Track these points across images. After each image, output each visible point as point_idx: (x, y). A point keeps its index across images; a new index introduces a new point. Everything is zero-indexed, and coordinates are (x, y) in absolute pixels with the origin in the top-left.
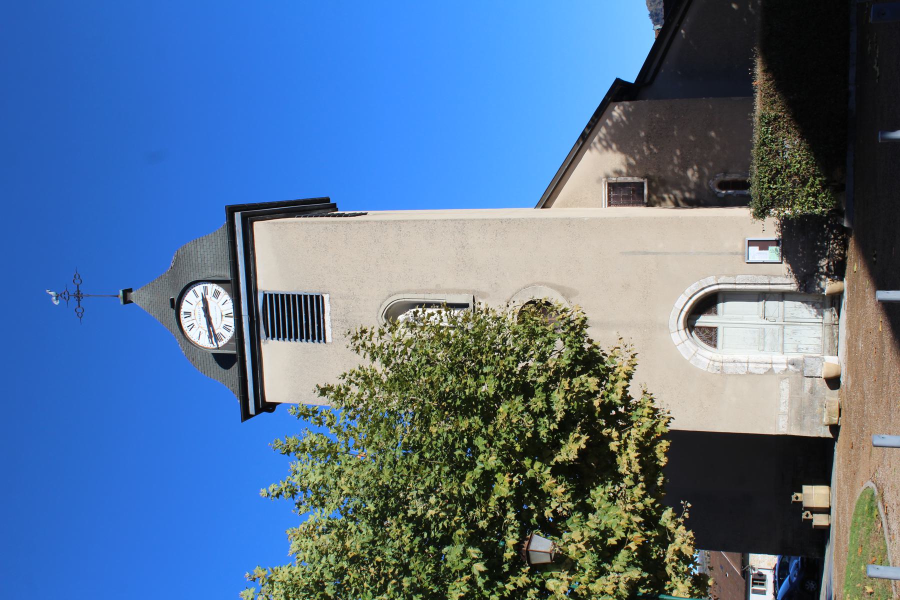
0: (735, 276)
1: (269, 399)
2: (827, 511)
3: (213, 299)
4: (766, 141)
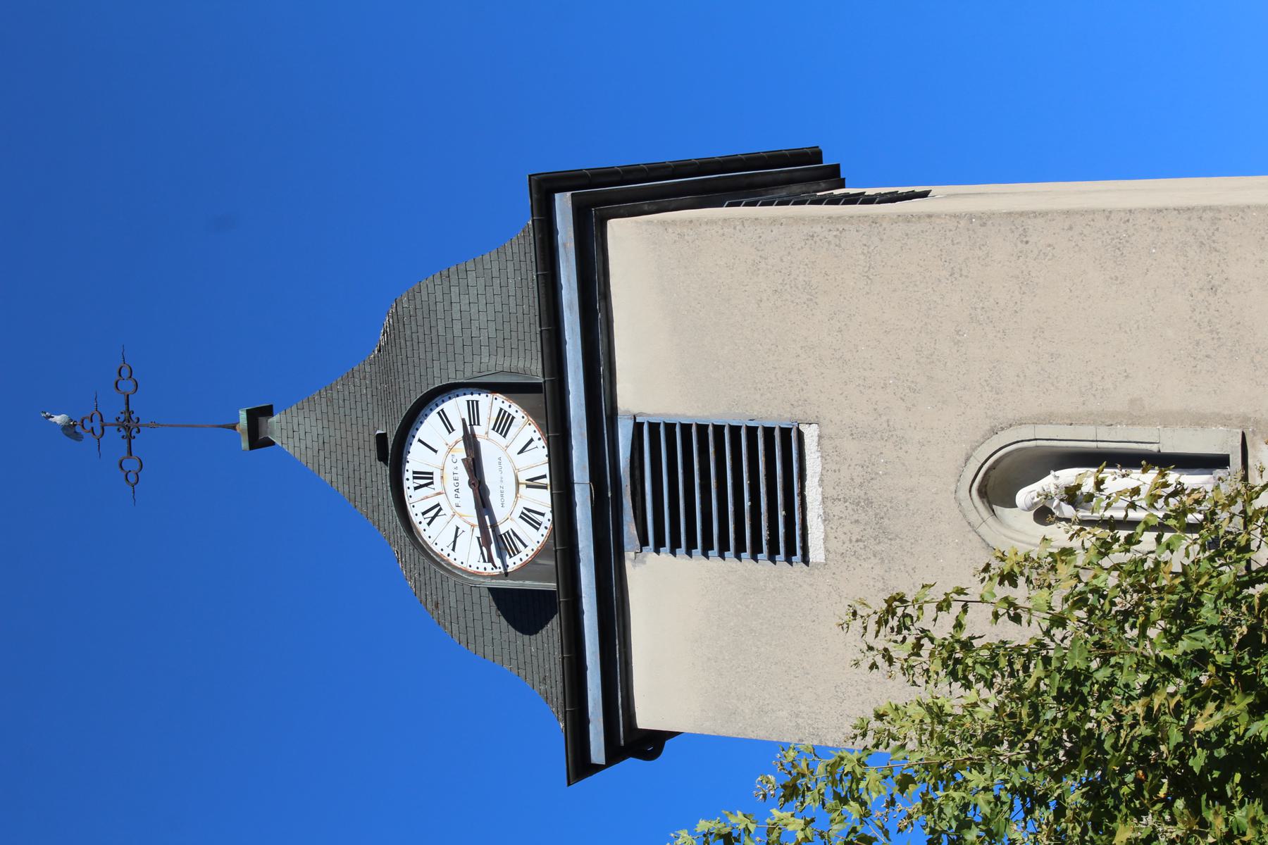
1: (644, 721)
3: (495, 436)
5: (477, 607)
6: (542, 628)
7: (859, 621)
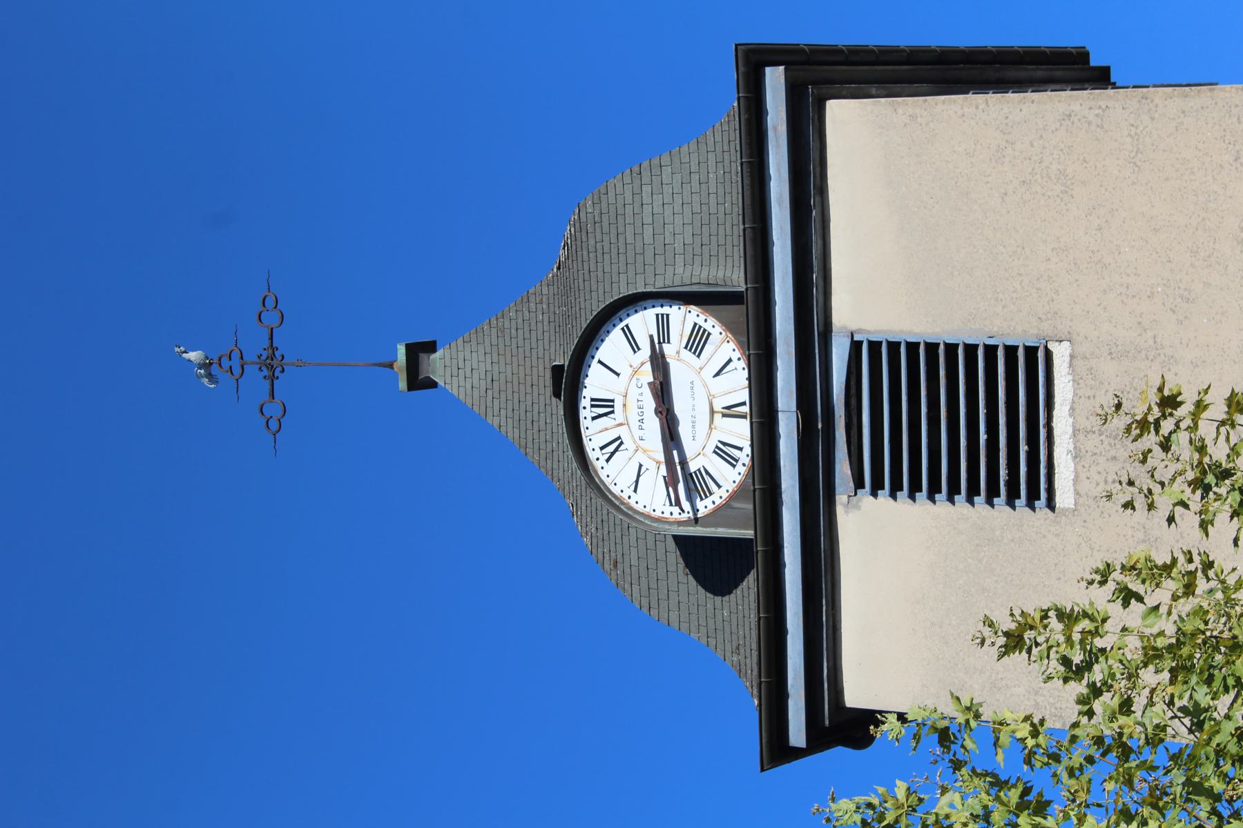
1: (854, 697)
3: (687, 355)
5: (661, 565)
6: (736, 587)
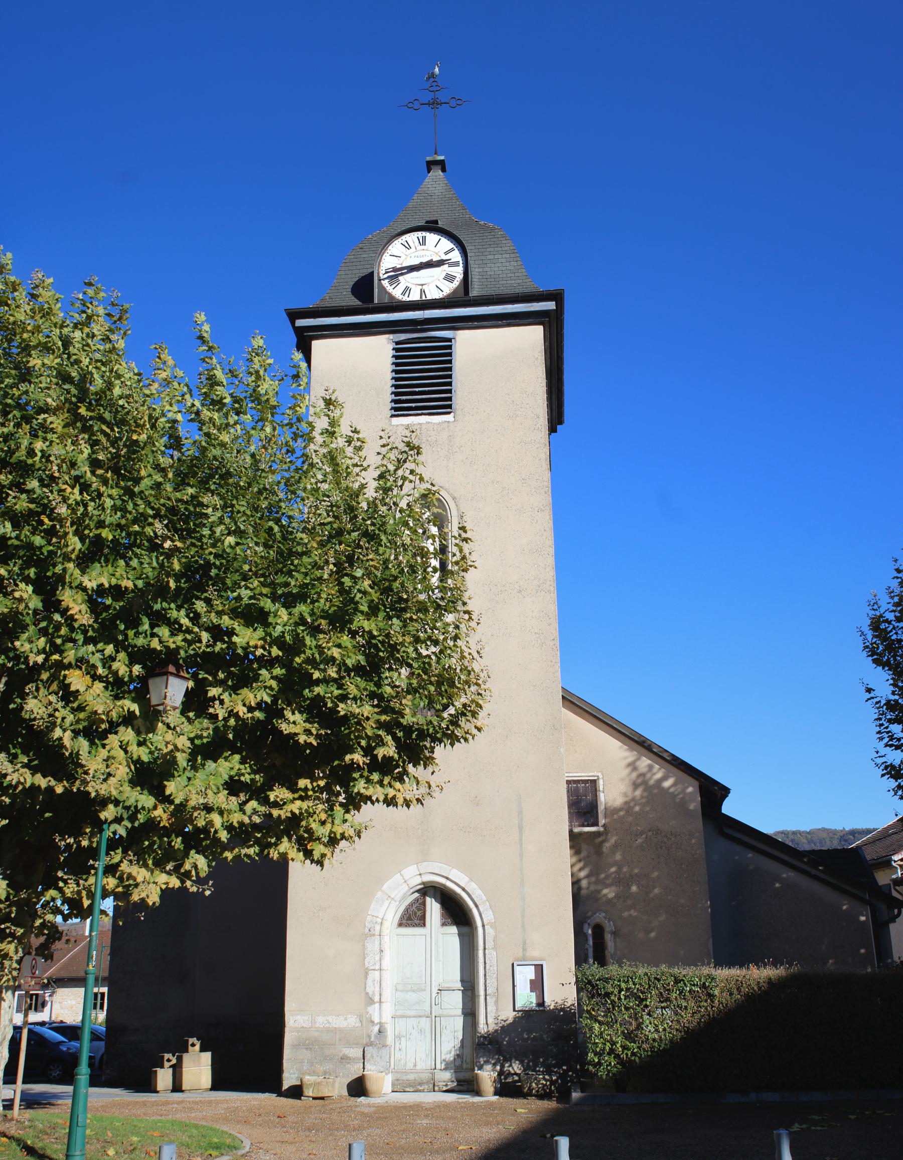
0: (495, 948)
2: (177, 1087)
4: (681, 984)
7: (408, 434)
